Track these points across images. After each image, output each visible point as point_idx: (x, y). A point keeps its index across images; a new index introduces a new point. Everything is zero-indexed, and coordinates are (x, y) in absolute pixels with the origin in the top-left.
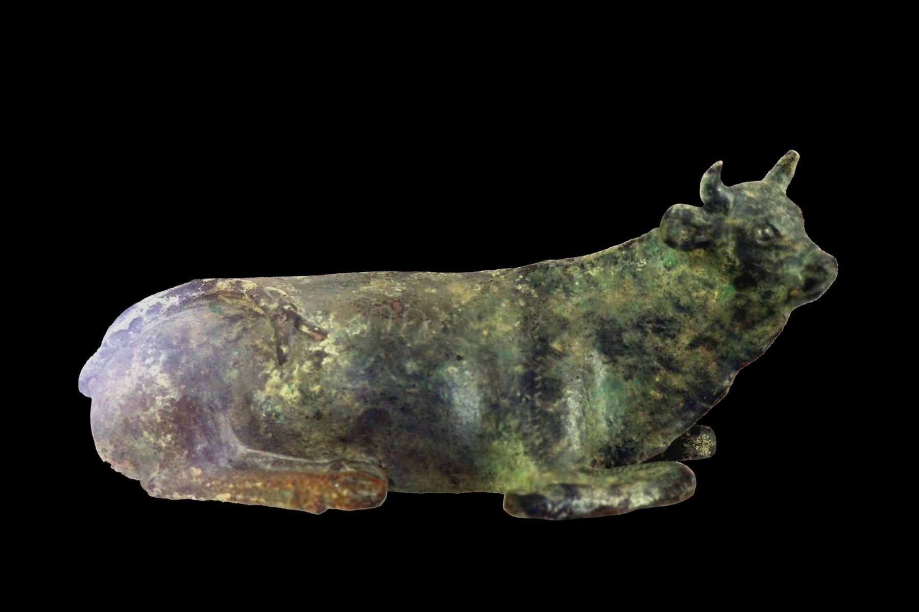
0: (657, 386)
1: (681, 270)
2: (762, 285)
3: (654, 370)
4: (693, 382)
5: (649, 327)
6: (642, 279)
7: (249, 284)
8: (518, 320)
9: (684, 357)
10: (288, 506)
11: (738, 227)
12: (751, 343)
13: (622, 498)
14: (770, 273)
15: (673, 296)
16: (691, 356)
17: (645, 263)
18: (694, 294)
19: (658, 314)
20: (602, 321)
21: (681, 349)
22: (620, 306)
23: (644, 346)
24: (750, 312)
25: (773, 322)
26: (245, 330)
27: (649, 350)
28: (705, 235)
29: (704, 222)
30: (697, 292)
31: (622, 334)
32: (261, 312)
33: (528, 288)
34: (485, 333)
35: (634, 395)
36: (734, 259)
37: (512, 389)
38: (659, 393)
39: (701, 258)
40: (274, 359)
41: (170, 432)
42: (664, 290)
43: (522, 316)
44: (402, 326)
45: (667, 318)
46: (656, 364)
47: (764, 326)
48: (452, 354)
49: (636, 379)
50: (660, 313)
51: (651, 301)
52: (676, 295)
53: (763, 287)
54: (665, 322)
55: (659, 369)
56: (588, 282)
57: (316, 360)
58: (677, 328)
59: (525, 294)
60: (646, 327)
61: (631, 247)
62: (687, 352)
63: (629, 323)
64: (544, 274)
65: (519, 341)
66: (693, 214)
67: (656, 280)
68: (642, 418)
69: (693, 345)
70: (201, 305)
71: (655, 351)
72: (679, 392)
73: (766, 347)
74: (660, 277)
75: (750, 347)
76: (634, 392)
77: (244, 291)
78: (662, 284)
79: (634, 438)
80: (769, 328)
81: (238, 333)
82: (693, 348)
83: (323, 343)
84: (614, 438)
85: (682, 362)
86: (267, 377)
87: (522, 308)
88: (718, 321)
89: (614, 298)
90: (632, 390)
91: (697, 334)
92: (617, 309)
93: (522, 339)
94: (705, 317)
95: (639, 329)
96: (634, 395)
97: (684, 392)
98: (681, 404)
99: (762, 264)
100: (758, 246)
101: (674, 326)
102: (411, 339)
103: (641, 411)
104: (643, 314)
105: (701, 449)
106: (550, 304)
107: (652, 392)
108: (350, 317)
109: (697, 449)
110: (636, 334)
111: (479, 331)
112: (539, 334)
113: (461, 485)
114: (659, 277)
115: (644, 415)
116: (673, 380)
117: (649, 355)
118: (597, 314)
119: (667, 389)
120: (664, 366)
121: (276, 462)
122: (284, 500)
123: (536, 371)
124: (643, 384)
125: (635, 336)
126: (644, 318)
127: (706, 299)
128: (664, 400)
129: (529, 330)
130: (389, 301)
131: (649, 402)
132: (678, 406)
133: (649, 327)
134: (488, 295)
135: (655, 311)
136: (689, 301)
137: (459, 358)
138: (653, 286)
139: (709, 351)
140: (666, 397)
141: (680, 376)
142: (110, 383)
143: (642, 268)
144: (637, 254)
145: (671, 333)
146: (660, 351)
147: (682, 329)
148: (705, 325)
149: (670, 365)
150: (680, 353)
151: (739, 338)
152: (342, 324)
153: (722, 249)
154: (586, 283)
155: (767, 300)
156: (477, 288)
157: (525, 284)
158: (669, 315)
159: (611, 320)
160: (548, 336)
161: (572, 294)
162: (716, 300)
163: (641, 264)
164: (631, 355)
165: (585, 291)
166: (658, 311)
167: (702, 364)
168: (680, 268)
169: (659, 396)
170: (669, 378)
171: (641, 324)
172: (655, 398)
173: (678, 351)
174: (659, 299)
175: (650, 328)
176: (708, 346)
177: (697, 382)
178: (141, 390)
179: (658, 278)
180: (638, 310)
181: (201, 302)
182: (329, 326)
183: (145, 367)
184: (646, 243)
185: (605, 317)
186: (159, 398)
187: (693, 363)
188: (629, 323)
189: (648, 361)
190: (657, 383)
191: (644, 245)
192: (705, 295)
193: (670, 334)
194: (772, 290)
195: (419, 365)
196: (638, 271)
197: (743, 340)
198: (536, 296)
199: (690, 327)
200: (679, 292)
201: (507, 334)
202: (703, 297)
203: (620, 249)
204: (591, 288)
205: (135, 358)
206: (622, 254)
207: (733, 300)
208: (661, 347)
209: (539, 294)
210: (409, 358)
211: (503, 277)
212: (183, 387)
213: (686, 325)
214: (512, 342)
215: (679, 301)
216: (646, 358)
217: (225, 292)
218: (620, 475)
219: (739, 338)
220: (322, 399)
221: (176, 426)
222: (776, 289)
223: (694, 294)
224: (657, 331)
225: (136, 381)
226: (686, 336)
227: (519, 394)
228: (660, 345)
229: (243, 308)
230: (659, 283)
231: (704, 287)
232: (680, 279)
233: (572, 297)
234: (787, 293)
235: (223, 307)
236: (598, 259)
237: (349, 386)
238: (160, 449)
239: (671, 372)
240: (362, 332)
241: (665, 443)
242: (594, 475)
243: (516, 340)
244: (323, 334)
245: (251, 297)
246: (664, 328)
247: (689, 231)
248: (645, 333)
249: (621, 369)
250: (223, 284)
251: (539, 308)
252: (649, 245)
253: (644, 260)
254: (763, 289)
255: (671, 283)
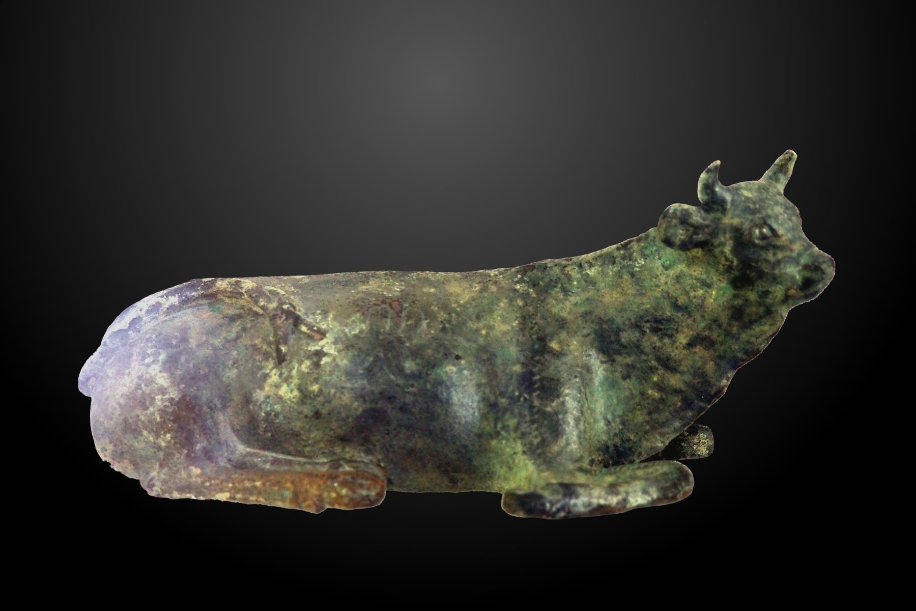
0: (655, 386)
1: (679, 269)
2: (759, 285)
3: (652, 369)
4: (690, 382)
5: (647, 327)
6: (640, 278)
7: (248, 283)
8: (516, 319)
9: (682, 356)
10: (287, 505)
11: (735, 227)
12: (748, 342)
13: (620, 497)
14: (767, 273)
15: (670, 295)
16: (689, 355)
17: (643, 263)
18: (692, 294)
19: (656, 314)
20: (600, 321)
21: (679, 348)
22: (618, 305)
23: (642, 346)
24: (748, 311)
25: (770, 322)
26: (244, 329)
27: (647, 350)
28: (703, 234)
29: (702, 221)
30: (695, 291)
31: (620, 333)
32: (261, 311)
33: (526, 288)
34: (484, 332)
35: (632, 394)
36: (732, 258)
37: (511, 388)
38: (657, 392)
39: (699, 258)
40: (273, 359)
41: (169, 431)
42: (662, 290)
43: (521, 315)
44: (401, 325)
45: (665, 317)
46: (654, 363)
47: (761, 325)
48: (450, 353)
49: (633, 378)
50: (658, 312)
51: (649, 301)
52: (674, 294)
53: (760, 286)
54: (663, 321)
55: (657, 369)
56: (586, 281)
57: (315, 359)
58: (675, 327)
59: (523, 293)
60: (644, 327)
61: (629, 246)
62: (685, 352)
63: (627, 323)
64: (542, 274)
65: (518, 340)
66: (691, 214)
67: (654, 280)
68: (640, 417)
69: (690, 345)
70: (201, 305)
71: (653, 350)
72: (677, 391)
73: (763, 347)
74: (658, 276)
75: (748, 347)
76: (632, 391)
77: (243, 291)
78: (660, 284)
79: (632, 437)
80: (766, 328)
81: (237, 332)
82: (691, 348)
83: (322, 343)
84: (612, 438)
85: (680, 361)
86: (266, 376)
87: (520, 307)
88: (715, 321)
89: (612, 298)
90: (630, 389)
91: (695, 333)
92: (615, 308)
93: (520, 338)
94: (703, 316)
95: (637, 329)
96: (632, 394)
97: (681, 391)
98: (679, 404)
99: (760, 263)
100: (755, 246)
101: (672, 326)
102: (410, 339)
103: (639, 410)
104: (641, 313)
105: (698, 448)
106: (548, 304)
107: (650, 392)
108: (349, 316)
109: (695, 448)
110: (634, 334)
111: (477, 331)
112: (537, 333)
113: (459, 484)
114: (656, 277)
115: (642, 415)
116: (671, 379)
117: (647, 354)
118: (595, 314)
119: (665, 389)
120: (662, 366)
121: (275, 462)
122: (283, 500)
123: (534, 370)
124: (641, 383)
125: (633, 336)
126: (642, 317)
127: (704, 299)
128: (662, 400)
129: (527, 329)
130: (388, 301)
131: (647, 401)
132: (676, 405)
133: (647, 327)
134: (486, 295)
135: (653, 311)
136: (687, 300)
137: (458, 358)
138: (651, 286)
139: (707, 350)
140: (664, 397)
141: (678, 376)
142: (109, 382)
143: (640, 267)
144: (635, 254)
145: (669, 332)
146: (658, 351)
147: (680, 328)
148: (703, 325)
149: (668, 364)
150: (677, 352)
151: (736, 338)
152: (341, 323)
153: (719, 249)
154: (584, 282)
155: (765, 300)
156: (476, 287)
157: (523, 284)
158: (666, 314)
159: (609, 320)
160: (546, 335)
161: (570, 293)
162: (714, 299)
163: (639, 263)
164: (629, 354)
165: (583, 290)
166: (656, 310)
167: (699, 364)
168: (678, 268)
169: (657, 395)
170: (667, 377)
171: (639, 324)
172: (653, 397)
173: (675, 351)
174: (657, 298)
175: (648, 328)
176: (705, 345)
177: (695, 381)
178: (141, 389)
179: (655, 278)
180: (636, 310)
181: (200, 302)
182: (328, 325)
183: (144, 367)
184: (644, 243)
185: (603, 316)
186: (159, 397)
187: (691, 363)
188: (627, 323)
189: (646, 361)
190: (655, 382)
191: (642, 244)
192: (703, 294)
193: (668, 333)
194: (770, 289)
195: (417, 364)
196: (636, 271)
197: (741, 339)
198: (534, 295)
199: (688, 326)
200: (677, 291)
201: (505, 333)
202: (701, 297)
203: (618, 249)
204: (589, 287)
205: (135, 357)
206: (620, 254)
207: (730, 300)
208: (659, 347)
209: (537, 294)
210: (407, 357)
211: (501, 276)
212: (182, 386)
213: (684, 324)
214: (510, 342)
215: (677, 300)
216: (644, 357)
217: (224, 292)
218: (618, 474)
219: (736, 338)
220: (321, 399)
221: (175, 426)
222: (773, 288)
223: (692, 294)
224: (655, 330)
225: (135, 381)
226: (684, 335)
227: (517, 394)
228: (658, 344)
229: (242, 307)
230: (657, 283)
231: (701, 287)
232: (678, 278)
233: (570, 296)
234: (784, 292)
235: (222, 307)
236: (596, 259)
237: (348, 385)
238: (159, 448)
239: (669, 371)
240: (361, 332)
241: (663, 442)
242: (592, 475)
243: (514, 340)
244: (322, 334)
245: (250, 296)
246: (662, 327)
247: (687, 230)
248: (643, 333)
249: (619, 368)
250: (222, 284)
251: (537, 307)
252: (647, 244)
253: (642, 259)
254: (761, 289)
255: (669, 283)
